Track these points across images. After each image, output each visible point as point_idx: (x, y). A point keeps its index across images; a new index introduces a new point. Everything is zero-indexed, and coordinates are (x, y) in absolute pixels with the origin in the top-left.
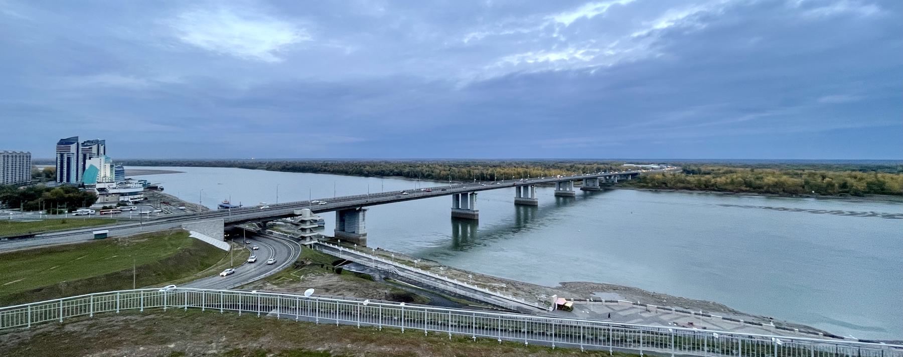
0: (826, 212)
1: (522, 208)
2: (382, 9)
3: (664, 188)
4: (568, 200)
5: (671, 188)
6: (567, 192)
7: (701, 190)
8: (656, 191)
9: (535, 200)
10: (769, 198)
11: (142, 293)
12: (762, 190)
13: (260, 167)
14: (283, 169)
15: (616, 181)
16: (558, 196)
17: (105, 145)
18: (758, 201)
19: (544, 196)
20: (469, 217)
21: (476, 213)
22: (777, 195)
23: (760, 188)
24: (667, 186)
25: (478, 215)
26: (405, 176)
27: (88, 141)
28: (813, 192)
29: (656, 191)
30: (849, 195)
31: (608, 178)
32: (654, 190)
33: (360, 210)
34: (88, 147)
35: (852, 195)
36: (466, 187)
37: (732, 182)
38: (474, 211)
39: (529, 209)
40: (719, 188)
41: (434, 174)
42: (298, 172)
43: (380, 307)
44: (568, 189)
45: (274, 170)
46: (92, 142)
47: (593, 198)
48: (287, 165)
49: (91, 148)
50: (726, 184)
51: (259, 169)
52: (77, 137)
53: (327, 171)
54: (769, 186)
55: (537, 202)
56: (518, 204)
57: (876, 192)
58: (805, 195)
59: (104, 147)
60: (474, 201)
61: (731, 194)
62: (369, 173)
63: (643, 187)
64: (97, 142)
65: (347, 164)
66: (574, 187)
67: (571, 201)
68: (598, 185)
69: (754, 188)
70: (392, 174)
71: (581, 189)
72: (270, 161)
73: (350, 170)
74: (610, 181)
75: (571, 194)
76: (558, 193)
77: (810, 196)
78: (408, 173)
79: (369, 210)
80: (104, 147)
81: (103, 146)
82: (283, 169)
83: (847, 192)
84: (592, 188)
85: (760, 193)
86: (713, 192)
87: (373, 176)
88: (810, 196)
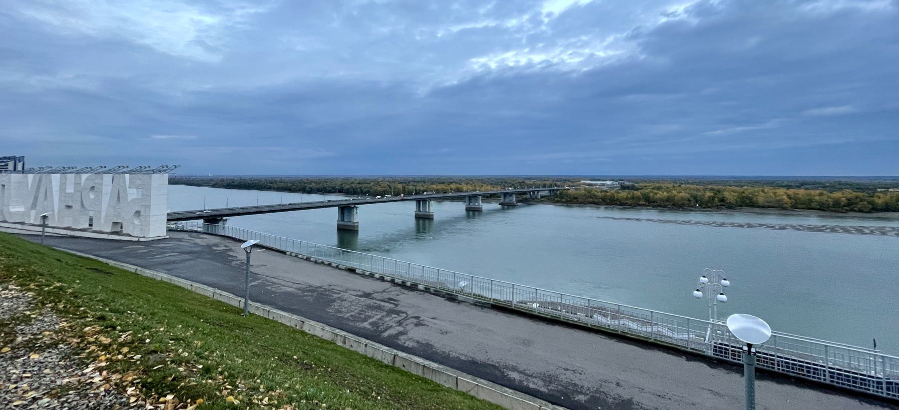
0: (633, 219)
1: (421, 221)
2: (439, 35)
3: (574, 203)
4: (477, 213)
5: (581, 203)
6: (475, 207)
7: (607, 204)
8: (567, 206)
9: (431, 214)
10: (662, 211)
11: (871, 388)
12: (656, 204)
13: (205, 184)
14: (228, 186)
15: (539, 197)
16: (468, 210)
17: (23, 161)
18: (653, 214)
19: (440, 210)
20: (351, 228)
21: (356, 224)
22: (666, 209)
23: (654, 202)
24: (578, 201)
25: (358, 226)
26: (345, 193)
27: (5, 158)
28: (698, 205)
29: (567, 205)
30: (724, 207)
31: (531, 193)
32: (565, 205)
33: (220, 220)
34: (3, 164)
35: (726, 208)
36: (350, 199)
37: (633, 198)
38: (354, 223)
39: (427, 222)
40: (621, 203)
41: (371, 191)
42: (243, 189)
43: (894, 386)
44: (476, 204)
45: (219, 187)
46: (9, 158)
47: (505, 212)
48: (233, 182)
49: (7, 165)
50: (627, 198)
51: (205, 186)
52: (24, 157)
53: (272, 189)
54: (662, 200)
55: (433, 215)
56: (418, 217)
57: (747, 206)
58: (690, 208)
59: (23, 164)
60: (355, 214)
61: (629, 208)
62: (311, 190)
63: (558, 202)
64: (13, 158)
65: (293, 183)
66: (482, 202)
67: (479, 215)
68: (514, 200)
69: (649, 202)
70: (333, 191)
71: (499, 204)
72: (222, 177)
73: (294, 187)
74: (534, 197)
75: (479, 208)
76: (469, 208)
77: (693, 209)
78: (348, 189)
79: (229, 220)
80: (23, 164)
81: (22, 162)
82: (228, 186)
83: (723, 205)
84: (509, 203)
85: (655, 207)
86: (615, 206)
87: (315, 193)
88: (693, 209)
